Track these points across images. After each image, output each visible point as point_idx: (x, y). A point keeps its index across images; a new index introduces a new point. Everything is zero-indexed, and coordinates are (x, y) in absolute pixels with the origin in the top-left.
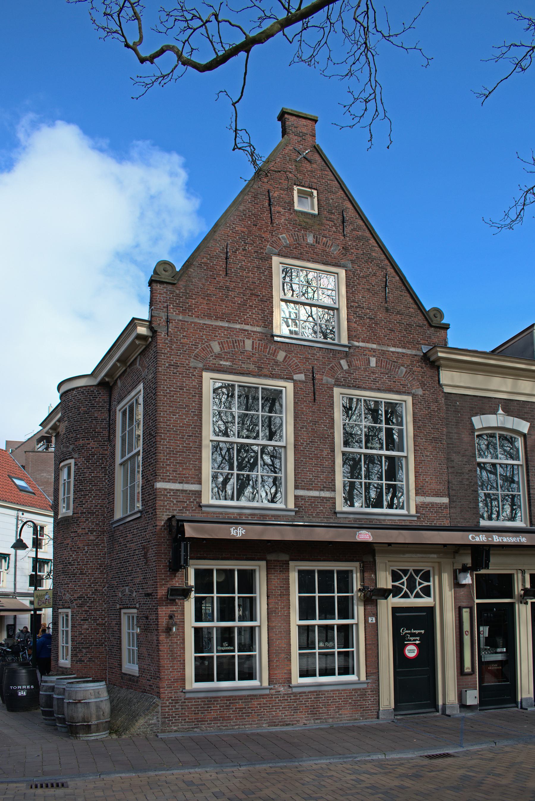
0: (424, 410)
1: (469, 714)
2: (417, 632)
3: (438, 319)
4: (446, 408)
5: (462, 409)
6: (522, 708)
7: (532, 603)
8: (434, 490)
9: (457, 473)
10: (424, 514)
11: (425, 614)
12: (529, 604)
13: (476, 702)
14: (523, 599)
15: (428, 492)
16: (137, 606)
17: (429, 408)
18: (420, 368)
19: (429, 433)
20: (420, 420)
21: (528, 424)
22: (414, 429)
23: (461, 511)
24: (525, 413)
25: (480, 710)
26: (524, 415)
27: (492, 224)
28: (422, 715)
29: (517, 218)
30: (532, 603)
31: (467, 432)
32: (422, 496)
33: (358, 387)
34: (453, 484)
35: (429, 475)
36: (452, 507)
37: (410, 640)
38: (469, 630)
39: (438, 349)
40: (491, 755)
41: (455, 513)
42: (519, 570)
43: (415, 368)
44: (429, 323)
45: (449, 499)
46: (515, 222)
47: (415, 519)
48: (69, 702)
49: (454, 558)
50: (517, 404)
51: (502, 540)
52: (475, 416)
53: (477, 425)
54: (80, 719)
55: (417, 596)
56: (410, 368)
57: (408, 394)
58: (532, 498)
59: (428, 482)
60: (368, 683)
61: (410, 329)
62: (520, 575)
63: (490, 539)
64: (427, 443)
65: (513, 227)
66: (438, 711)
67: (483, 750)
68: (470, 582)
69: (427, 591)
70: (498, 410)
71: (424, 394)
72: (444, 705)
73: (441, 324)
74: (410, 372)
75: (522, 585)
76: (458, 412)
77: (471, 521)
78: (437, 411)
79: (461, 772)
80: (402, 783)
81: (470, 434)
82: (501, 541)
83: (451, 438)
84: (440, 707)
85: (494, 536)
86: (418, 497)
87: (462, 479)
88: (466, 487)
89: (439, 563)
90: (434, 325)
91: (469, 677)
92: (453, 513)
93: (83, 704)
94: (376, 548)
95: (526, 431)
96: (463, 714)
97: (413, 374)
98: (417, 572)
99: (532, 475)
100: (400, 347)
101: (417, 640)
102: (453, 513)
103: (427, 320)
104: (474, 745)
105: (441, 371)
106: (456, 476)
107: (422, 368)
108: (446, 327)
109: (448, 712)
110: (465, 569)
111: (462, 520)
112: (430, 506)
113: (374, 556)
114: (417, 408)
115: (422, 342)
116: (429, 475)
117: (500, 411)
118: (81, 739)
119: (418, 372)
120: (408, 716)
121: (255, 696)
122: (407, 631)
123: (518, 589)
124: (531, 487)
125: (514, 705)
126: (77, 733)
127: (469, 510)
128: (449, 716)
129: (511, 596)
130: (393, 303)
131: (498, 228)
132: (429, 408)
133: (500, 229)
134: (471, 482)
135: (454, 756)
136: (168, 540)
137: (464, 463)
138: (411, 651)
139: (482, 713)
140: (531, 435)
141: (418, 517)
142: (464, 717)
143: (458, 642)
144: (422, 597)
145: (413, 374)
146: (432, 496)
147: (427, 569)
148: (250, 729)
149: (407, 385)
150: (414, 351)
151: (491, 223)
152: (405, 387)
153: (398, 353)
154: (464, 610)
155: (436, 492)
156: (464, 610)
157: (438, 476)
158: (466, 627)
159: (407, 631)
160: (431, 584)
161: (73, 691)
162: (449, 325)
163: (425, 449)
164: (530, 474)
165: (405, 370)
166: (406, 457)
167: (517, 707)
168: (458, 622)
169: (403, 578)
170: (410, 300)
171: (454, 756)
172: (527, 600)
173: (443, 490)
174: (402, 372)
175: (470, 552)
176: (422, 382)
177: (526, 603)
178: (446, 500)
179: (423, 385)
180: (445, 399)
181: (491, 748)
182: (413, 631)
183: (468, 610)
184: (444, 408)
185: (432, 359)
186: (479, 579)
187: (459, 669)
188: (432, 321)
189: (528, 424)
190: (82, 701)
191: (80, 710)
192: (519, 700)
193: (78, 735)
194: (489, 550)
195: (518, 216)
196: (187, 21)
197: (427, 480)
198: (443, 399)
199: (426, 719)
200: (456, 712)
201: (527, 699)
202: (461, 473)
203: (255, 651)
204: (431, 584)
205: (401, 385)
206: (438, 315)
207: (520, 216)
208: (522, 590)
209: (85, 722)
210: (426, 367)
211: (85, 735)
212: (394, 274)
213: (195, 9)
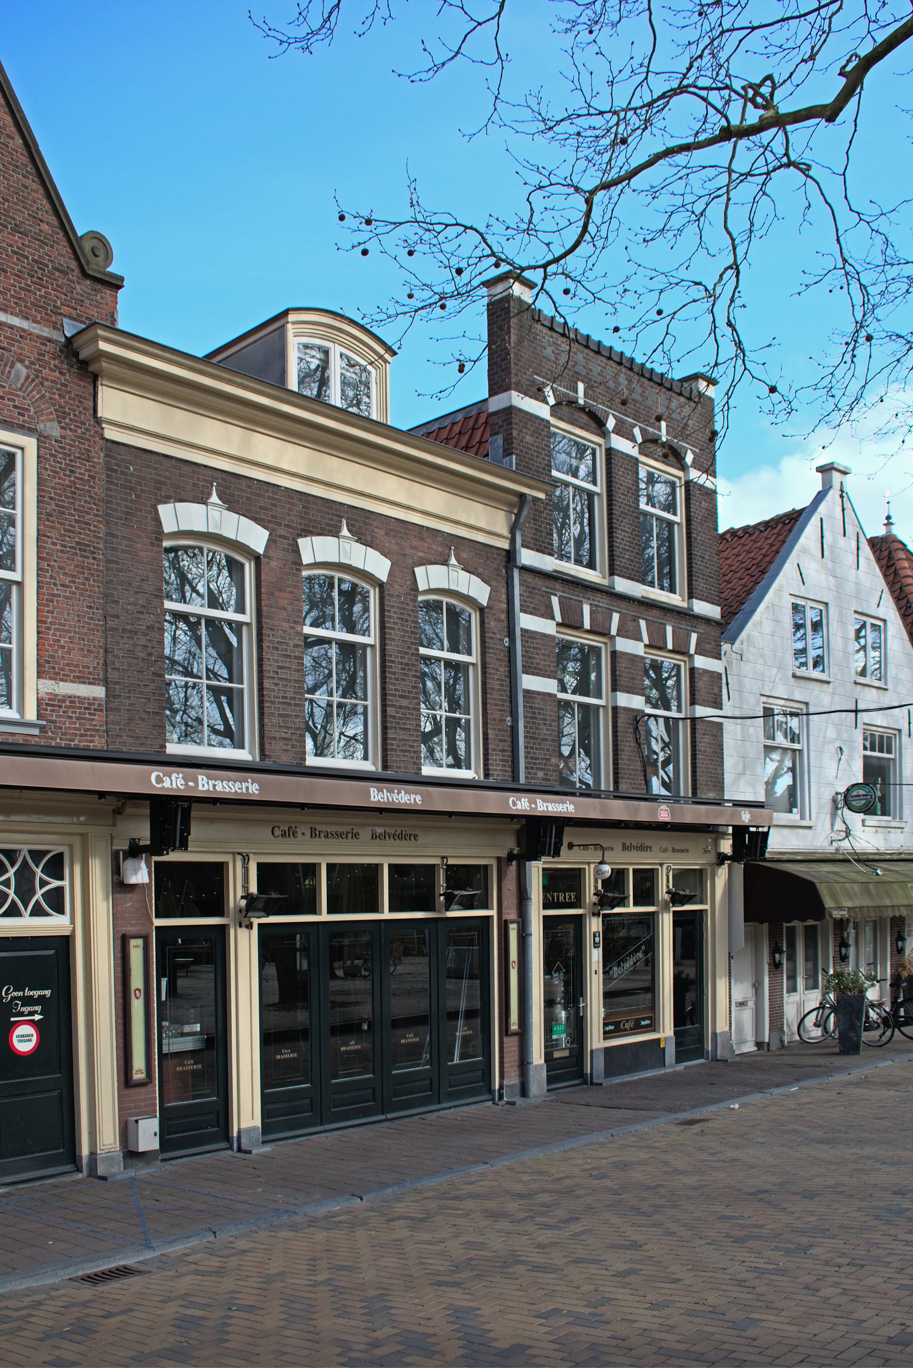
0: (62, 475)
1: (142, 1172)
2: (36, 993)
3: (101, 259)
4: (108, 476)
5: (139, 484)
6: (240, 1150)
7: (259, 924)
8: (77, 666)
9: (124, 630)
10: (55, 722)
11: (52, 952)
12: (255, 931)
13: (155, 1145)
14: (245, 916)
15: (63, 670)
17: (71, 471)
18: (57, 374)
19: (69, 531)
20: (51, 498)
21: (264, 534)
22: (38, 519)
23: (131, 719)
24: (261, 507)
25: (163, 1160)
26: (259, 513)
27: (270, 32)
28: (48, 1181)
29: (323, 27)
30: (259, 924)
31: (147, 537)
32: (51, 678)
34: (115, 656)
35: (68, 631)
36: (111, 709)
37: (22, 1014)
38: (141, 987)
39: (100, 332)
40: (214, 1262)
41: (118, 724)
42: (239, 854)
43: (47, 370)
44: (81, 266)
45: (107, 691)
46: (316, 37)
47: (36, 732)
49: (114, 825)
50: (248, 486)
51: (214, 786)
52: (165, 503)
53: (169, 526)
55: (38, 911)
56: (36, 370)
57: (29, 431)
58: (266, 698)
59: (63, 647)
61: (40, 272)
62: (239, 864)
63: (191, 784)
64: (65, 555)
65: (312, 48)
66: (79, 1170)
67: (193, 1251)
68: (146, 880)
69: (56, 901)
70: (209, 495)
71: (63, 437)
72: (93, 1154)
73: (106, 274)
74: (36, 378)
75: (243, 886)
76: (132, 489)
77: (148, 742)
78: (89, 481)
79: (172, 1310)
80: (57, 1352)
81: (152, 544)
82: (211, 789)
83: (114, 549)
84: (85, 1161)
85: (200, 777)
86: (42, 681)
87: (134, 645)
88: (141, 665)
89: (83, 836)
90: (91, 273)
91: (142, 1090)
92: (113, 723)
95: (260, 549)
96: (131, 1173)
97: (42, 384)
98: (37, 855)
99: (268, 647)
100: (17, 315)
101: (36, 1012)
102: (113, 723)
103: (77, 258)
104: (175, 1241)
105: (100, 387)
106: (122, 637)
107: (60, 373)
108: (115, 284)
109: (101, 1171)
110: (135, 851)
111: (131, 740)
112: (68, 703)
114: (46, 469)
115: (64, 310)
116: (68, 631)
117: (214, 498)
119: (52, 381)
120: (21, 1186)
122: (16, 994)
123: (235, 897)
124: (265, 674)
125: (224, 1145)
127: (146, 717)
128: (104, 1178)
129: (219, 911)
130: (8, 201)
131: (282, 42)
132: (71, 471)
133: (285, 45)
134: (151, 654)
135: (140, 1272)
137: (139, 608)
138: (25, 1038)
139: (168, 1166)
140: (269, 558)
141: (42, 728)
142: (133, 1178)
143: (121, 1014)
144: (47, 915)
145: (42, 384)
146: (71, 681)
147: (57, 849)
149: (29, 410)
150: (46, 329)
151: (266, 29)
152: (23, 415)
153: (11, 327)
154: (133, 942)
155: (80, 672)
156: (133, 942)
157: (85, 634)
158: (137, 980)
159: (16, 994)
160: (66, 883)
162: (122, 279)
163: (60, 568)
164: (265, 645)
165: (24, 372)
166: (20, 584)
167: (231, 1148)
168: (119, 969)
169: (7, 871)
170: (45, 202)
171: (140, 1272)
172: (252, 919)
173: (95, 668)
174: (18, 376)
175: (147, 811)
176: (61, 407)
177: (250, 926)
178: (99, 692)
179: (61, 415)
180: (106, 456)
181: (208, 1245)
182: (28, 993)
183: (140, 942)
184: (104, 477)
185: (83, 355)
186: (162, 872)
187: (122, 1074)
188: (88, 263)
189: (264, 534)
192: (235, 1134)
194: (189, 808)
195: (325, 22)
197: (62, 643)
198: (102, 455)
199: (58, 1191)
200: (116, 1169)
201: (250, 1130)
202: (130, 632)
204: (66, 883)
205: (15, 407)
206: (101, 253)
207: (327, 25)
208: (242, 897)
210: (69, 371)
212: (13, 129)
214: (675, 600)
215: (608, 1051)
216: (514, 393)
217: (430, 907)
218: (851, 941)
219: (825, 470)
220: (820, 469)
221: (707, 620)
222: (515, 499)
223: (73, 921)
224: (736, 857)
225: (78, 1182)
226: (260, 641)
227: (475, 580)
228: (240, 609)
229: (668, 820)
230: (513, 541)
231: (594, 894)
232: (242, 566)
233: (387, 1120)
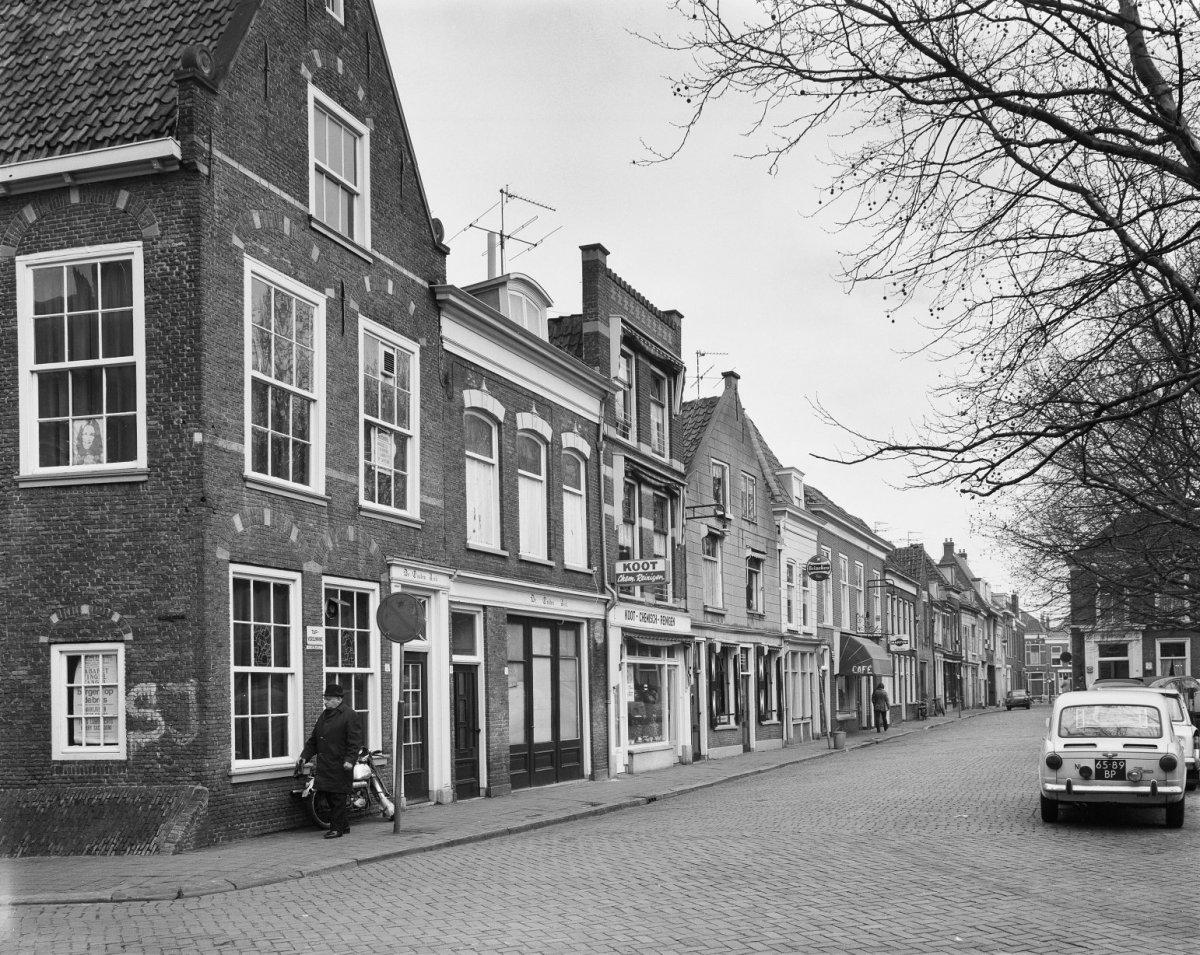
16: (129, 637)
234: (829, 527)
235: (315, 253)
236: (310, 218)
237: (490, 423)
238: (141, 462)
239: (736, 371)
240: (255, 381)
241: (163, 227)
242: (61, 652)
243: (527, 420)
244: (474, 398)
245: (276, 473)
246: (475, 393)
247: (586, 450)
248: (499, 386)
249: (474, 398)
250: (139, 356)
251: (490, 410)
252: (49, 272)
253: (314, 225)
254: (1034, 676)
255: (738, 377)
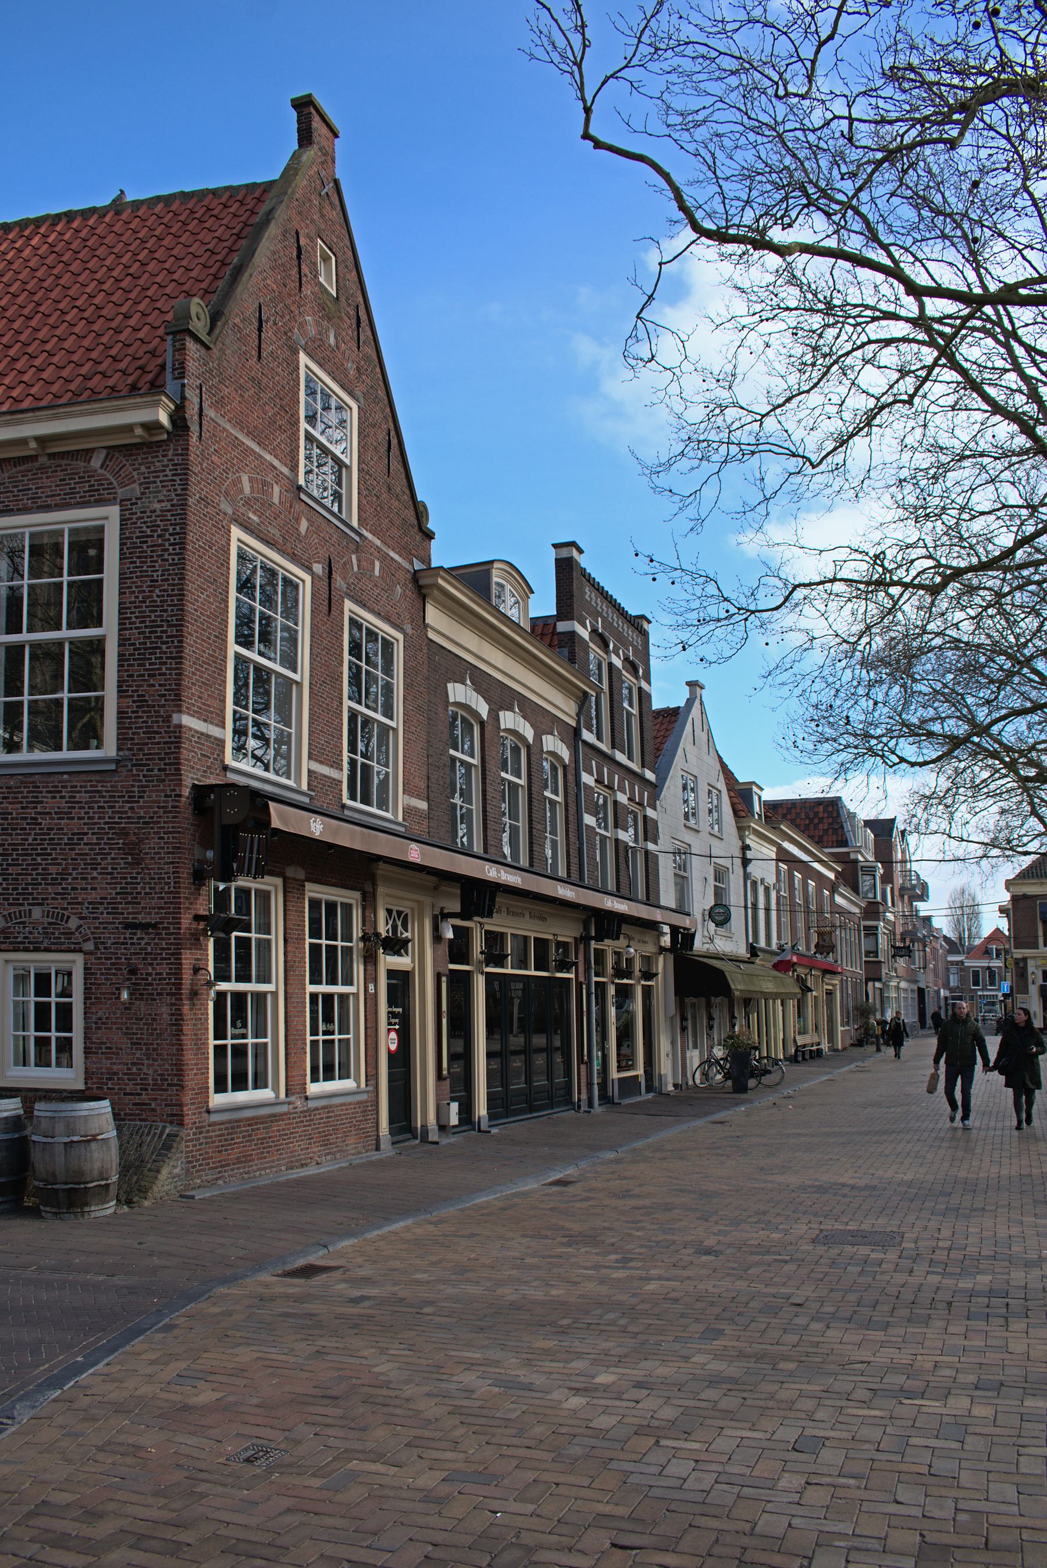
1: (453, 1139)
6: (479, 1131)
16: (89, 946)
33: (365, 605)
48: (72, 1142)
54: (96, 1173)
60: (368, 1092)
66: (415, 1137)
93: (100, 1143)
94: (379, 872)
113: (374, 885)
118: (93, 1215)
121: (274, 1115)
126: (86, 1204)
136: (192, 825)
148: (265, 1177)
158: (444, 1007)
161: (80, 1117)
175: (459, 891)
185: (422, 582)
190: (99, 1137)
191: (96, 1155)
193: (87, 1209)
196: (933, 402)
203: (266, 1037)
209: (102, 1180)
211: (100, 1207)
213: (586, 136)
214: (634, 766)
215: (620, 1079)
216: (576, 624)
217: (547, 970)
218: (689, 1017)
219: (693, 685)
220: (689, 684)
221: (648, 781)
222: (581, 694)
223: (413, 961)
224: (673, 949)
225: (414, 1147)
226: (484, 778)
227: (528, 725)
228: (518, 774)
229: (418, 861)
230: (578, 722)
231: (481, 953)
232: (472, 726)
233: (533, 1118)
234: (786, 845)
235: (304, 525)
236: (300, 488)
237: (473, 722)
238: (110, 749)
239: (702, 681)
240: (238, 656)
241: (146, 484)
242: (7, 961)
243: (509, 719)
244: (459, 692)
245: (379, 807)
246: (509, 714)
247: (565, 754)
248: (483, 683)
249: (459, 692)
250: (109, 629)
251: (521, 732)
252: (75, 554)
253: (303, 496)
254: (48, 917)
255: (702, 688)
